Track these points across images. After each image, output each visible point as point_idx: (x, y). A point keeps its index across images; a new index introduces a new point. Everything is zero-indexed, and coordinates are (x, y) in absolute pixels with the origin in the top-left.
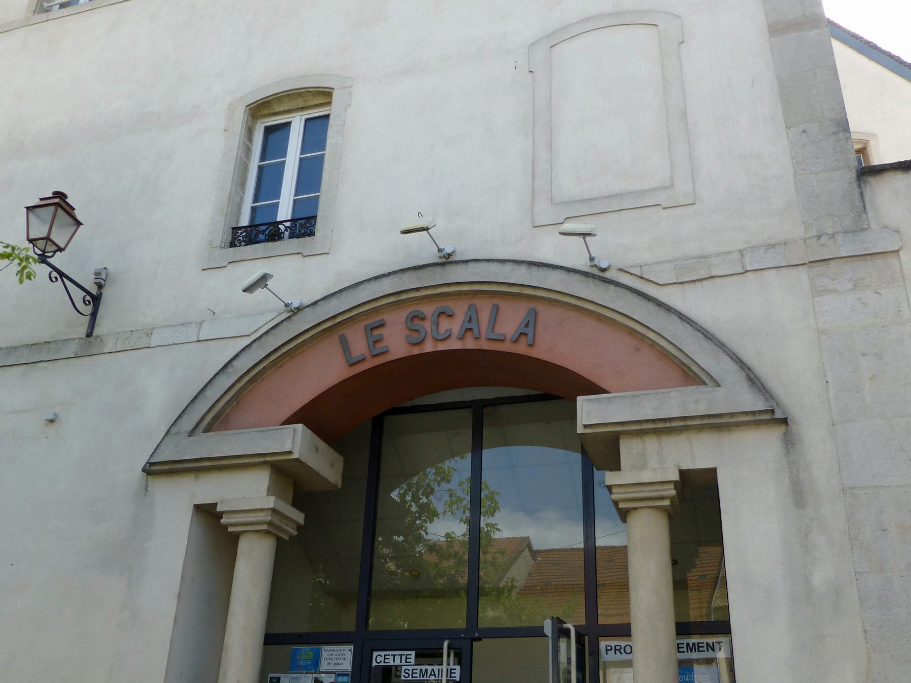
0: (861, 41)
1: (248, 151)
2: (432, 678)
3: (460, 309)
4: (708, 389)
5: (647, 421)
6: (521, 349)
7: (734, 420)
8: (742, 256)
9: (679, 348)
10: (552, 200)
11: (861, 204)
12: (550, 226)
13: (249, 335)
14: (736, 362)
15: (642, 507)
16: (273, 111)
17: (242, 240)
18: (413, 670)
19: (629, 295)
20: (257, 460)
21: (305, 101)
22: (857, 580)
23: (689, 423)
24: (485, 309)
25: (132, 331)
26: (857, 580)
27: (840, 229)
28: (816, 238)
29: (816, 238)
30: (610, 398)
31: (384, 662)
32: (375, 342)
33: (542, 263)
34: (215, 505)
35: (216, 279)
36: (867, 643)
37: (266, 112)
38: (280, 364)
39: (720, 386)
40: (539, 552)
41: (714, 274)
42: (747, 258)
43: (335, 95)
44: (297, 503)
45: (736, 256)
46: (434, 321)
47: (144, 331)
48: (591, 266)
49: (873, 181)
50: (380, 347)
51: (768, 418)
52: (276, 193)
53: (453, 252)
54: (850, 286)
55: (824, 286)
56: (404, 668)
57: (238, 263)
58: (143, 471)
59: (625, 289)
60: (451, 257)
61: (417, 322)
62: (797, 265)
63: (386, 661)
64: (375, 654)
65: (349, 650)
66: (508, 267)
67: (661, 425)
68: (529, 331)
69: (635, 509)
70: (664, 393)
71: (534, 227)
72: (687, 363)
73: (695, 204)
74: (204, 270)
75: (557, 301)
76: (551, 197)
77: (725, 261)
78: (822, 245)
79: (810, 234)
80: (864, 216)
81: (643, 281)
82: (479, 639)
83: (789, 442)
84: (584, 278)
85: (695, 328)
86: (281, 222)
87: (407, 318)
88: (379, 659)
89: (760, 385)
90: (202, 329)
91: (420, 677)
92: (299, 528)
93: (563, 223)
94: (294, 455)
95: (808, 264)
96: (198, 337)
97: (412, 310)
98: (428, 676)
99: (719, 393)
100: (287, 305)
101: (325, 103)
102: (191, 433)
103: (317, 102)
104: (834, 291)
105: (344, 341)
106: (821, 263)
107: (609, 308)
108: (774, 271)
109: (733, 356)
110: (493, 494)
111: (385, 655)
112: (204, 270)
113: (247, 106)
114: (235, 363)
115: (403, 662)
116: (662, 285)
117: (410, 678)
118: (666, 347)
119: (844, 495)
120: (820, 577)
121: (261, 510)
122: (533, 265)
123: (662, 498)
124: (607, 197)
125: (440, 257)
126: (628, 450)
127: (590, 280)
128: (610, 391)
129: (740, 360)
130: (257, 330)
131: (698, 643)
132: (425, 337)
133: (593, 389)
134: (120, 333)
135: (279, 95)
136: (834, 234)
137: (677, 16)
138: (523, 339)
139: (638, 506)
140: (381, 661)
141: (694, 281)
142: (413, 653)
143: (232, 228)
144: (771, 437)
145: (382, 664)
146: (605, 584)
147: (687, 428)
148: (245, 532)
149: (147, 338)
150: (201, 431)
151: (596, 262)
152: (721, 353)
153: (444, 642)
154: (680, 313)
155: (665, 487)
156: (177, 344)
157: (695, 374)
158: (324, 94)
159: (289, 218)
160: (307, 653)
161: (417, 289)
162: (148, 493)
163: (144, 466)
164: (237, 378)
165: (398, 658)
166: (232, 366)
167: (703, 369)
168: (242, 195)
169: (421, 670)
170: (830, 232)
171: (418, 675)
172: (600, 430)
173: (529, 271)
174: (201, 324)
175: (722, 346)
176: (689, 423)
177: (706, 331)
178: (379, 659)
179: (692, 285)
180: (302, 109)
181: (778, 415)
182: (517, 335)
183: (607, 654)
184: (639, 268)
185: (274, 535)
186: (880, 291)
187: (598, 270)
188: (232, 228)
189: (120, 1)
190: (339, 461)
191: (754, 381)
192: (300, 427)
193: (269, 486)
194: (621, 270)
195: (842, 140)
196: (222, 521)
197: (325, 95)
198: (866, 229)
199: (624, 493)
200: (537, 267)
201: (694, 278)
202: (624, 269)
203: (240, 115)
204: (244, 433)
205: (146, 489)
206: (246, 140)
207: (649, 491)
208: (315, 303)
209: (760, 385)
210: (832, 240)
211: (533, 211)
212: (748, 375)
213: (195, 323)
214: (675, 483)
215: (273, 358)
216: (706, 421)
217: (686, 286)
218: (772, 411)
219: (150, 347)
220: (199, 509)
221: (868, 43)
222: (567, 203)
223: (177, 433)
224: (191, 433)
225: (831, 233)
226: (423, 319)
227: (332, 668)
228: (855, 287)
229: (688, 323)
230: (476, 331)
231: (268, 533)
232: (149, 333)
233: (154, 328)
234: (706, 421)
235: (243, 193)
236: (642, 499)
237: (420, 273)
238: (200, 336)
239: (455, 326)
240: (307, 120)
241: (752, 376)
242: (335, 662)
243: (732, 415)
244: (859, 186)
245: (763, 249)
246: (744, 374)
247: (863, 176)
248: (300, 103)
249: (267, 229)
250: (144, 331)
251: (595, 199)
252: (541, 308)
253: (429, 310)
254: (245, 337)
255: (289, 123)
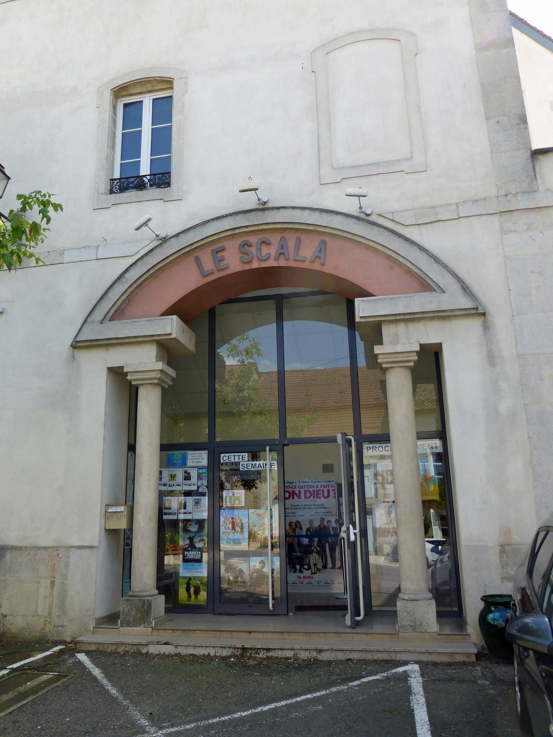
0: (516, 18)
1: (114, 122)
2: (260, 469)
3: (275, 239)
4: (438, 294)
5: (400, 314)
6: (316, 266)
7: (453, 313)
8: (458, 207)
9: (419, 268)
10: (332, 165)
11: (533, 174)
12: (332, 184)
13: (132, 256)
14: (455, 277)
15: (396, 367)
16: (129, 93)
17: (118, 188)
18: (247, 464)
19: (386, 233)
20: (148, 339)
21: (152, 86)
22: (525, 408)
23: (426, 315)
24: (291, 239)
25: (49, 252)
26: (525, 408)
27: (519, 191)
28: (505, 197)
29: (505, 197)
30: (376, 299)
31: (228, 460)
32: (220, 261)
33: (328, 210)
34: (122, 367)
35: (104, 217)
36: (531, 444)
37: (125, 93)
38: (156, 275)
39: (445, 293)
40: (262, 373)
41: (440, 218)
42: (461, 208)
43: (175, 83)
44: (170, 363)
45: (454, 207)
46: (258, 248)
47: (58, 252)
48: (360, 212)
49: (541, 158)
50: (223, 264)
51: (474, 312)
52: (138, 154)
53: (268, 201)
54: (525, 228)
55: (509, 228)
56: (241, 463)
57: (118, 205)
58: (71, 346)
59: (384, 229)
60: (266, 204)
61: (246, 248)
62: (492, 214)
63: (229, 459)
64: (222, 455)
65: (205, 453)
66: (307, 213)
67: (408, 317)
68: (322, 255)
69: (392, 367)
70: (410, 296)
71: (321, 184)
72: (424, 278)
73: (427, 171)
74: (94, 209)
75: (339, 235)
76: (332, 164)
77: (446, 210)
78: (508, 201)
79: (500, 194)
80: (535, 182)
81: (394, 222)
82: (288, 445)
83: (486, 327)
84: (357, 221)
85: (428, 255)
86: (145, 176)
87: (240, 245)
88: (225, 458)
89: (469, 292)
90: (99, 251)
91: (252, 468)
92: (173, 380)
93: (340, 182)
94: (173, 335)
95: (499, 214)
96: (97, 257)
97: (242, 241)
98: (257, 467)
99: (444, 296)
100: (157, 236)
101: (167, 88)
102: (102, 322)
103: (161, 87)
104: (515, 231)
105: (198, 260)
106: (508, 213)
107: (374, 241)
108: (477, 217)
109: (453, 274)
110: (257, 344)
111: (228, 456)
112: (94, 209)
113: (111, 90)
114: (126, 275)
115: (241, 460)
116: (407, 226)
117: (246, 469)
118: (409, 267)
119: (519, 359)
120: (503, 408)
121: (153, 371)
122: (323, 212)
123: (409, 361)
124: (368, 165)
125: (259, 204)
126: (387, 331)
127: (361, 222)
128: (371, 291)
129: (457, 275)
130: (138, 252)
131: (423, 444)
132: (252, 258)
133: (365, 294)
134: (41, 253)
135: (134, 82)
136: (516, 194)
137: (413, 35)
138: (318, 260)
139: (394, 366)
140: (226, 460)
141: (427, 223)
142: (246, 454)
143: (110, 179)
144: (476, 323)
145: (227, 461)
146: (312, 394)
147: (424, 318)
148: (142, 384)
149: (61, 257)
150: (108, 320)
151: (363, 210)
152: (445, 271)
153: (266, 448)
154: (419, 245)
155: (411, 354)
156: (82, 261)
157: (429, 284)
158: (166, 82)
159: (149, 174)
160: (178, 456)
161: (247, 226)
162: (75, 360)
163: (72, 343)
164: (129, 285)
165: (237, 458)
166: (125, 278)
167: (434, 281)
168: (114, 154)
169: (252, 464)
170: (513, 192)
171: (250, 467)
172: (370, 320)
173: (320, 216)
174: (98, 247)
175: (445, 267)
176: (426, 315)
177: (435, 257)
178: (225, 458)
179: (425, 226)
180: (150, 92)
181: (480, 310)
182: (314, 258)
183: (368, 452)
184: (391, 214)
185: (160, 385)
186: (543, 232)
187: (365, 215)
188: (110, 179)
189: (4, 2)
190: (193, 335)
191: (466, 289)
192: (175, 317)
193: (156, 355)
194: (379, 215)
195: (522, 129)
196: (128, 378)
197: (168, 83)
198: (536, 191)
199: (386, 358)
200: (326, 213)
201: (427, 222)
202: (382, 215)
203: (108, 96)
204: (138, 321)
205: (73, 357)
206: (113, 115)
207: (401, 357)
208: (177, 235)
209: (469, 292)
210: (515, 198)
211: (319, 173)
212: (462, 286)
213: (93, 247)
214: (417, 352)
215: (151, 272)
216: (436, 314)
217: (421, 226)
218: (477, 309)
219: (63, 263)
220: (111, 370)
221: (521, 20)
222: (343, 168)
223: (92, 322)
224: (102, 322)
225: (514, 193)
226: (250, 246)
227: (195, 464)
228: (529, 229)
229: (424, 252)
230: (286, 255)
231: (157, 384)
232: (62, 254)
233: (65, 250)
234: (436, 314)
235: (114, 154)
236: (396, 362)
237: (248, 215)
238: (98, 256)
239: (273, 250)
240: (154, 100)
241: (465, 286)
242: (197, 460)
243: (452, 310)
244: (533, 161)
245: (471, 203)
246: (460, 285)
247: (535, 155)
248: (149, 87)
249: (136, 180)
250: (58, 252)
251: (361, 166)
252: (328, 239)
253: (254, 240)
254: (129, 257)
255: (142, 102)
